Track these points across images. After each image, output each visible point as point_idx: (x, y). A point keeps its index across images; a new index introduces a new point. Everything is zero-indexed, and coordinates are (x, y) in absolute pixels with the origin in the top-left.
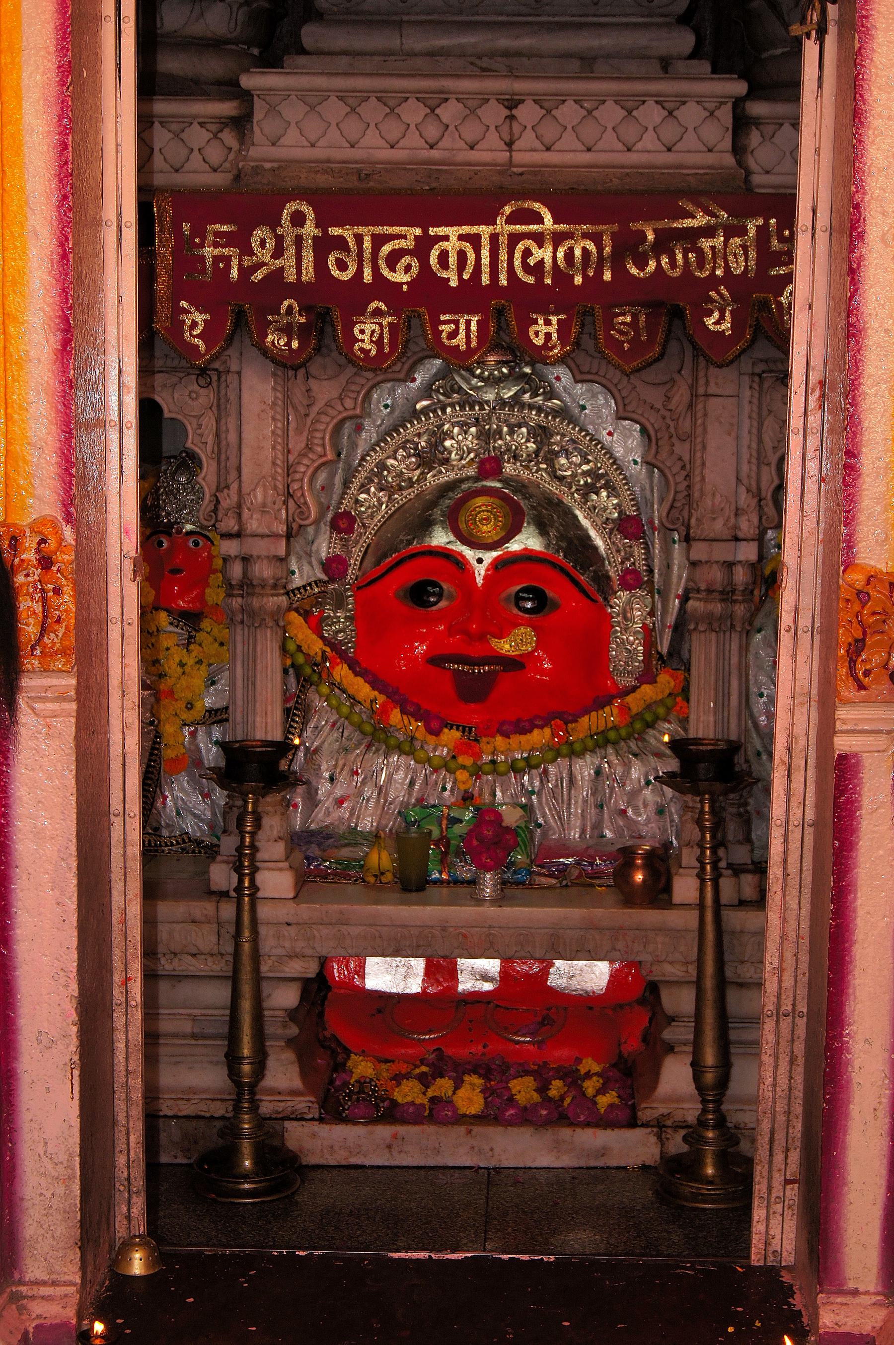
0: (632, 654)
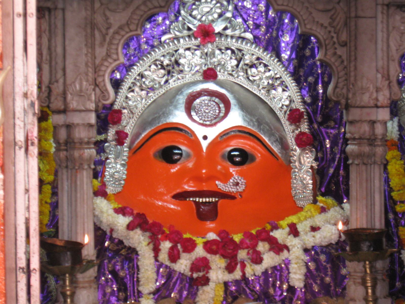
0: (305, 186)
